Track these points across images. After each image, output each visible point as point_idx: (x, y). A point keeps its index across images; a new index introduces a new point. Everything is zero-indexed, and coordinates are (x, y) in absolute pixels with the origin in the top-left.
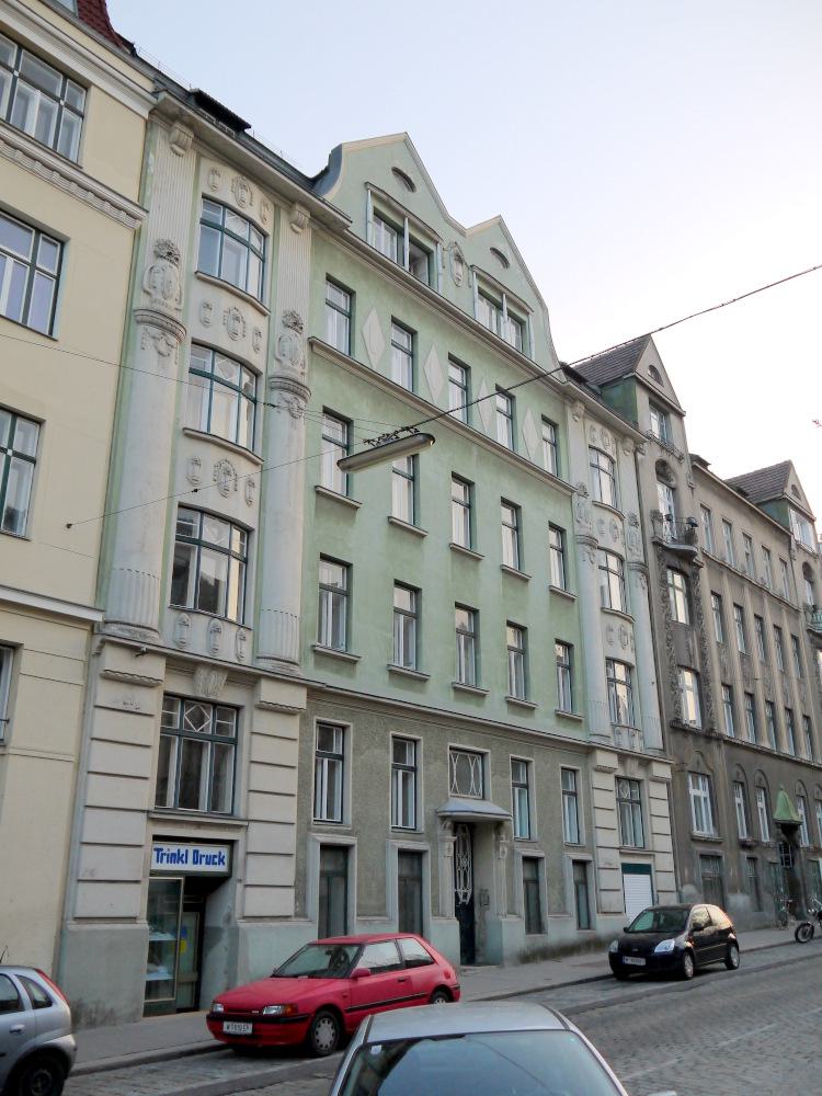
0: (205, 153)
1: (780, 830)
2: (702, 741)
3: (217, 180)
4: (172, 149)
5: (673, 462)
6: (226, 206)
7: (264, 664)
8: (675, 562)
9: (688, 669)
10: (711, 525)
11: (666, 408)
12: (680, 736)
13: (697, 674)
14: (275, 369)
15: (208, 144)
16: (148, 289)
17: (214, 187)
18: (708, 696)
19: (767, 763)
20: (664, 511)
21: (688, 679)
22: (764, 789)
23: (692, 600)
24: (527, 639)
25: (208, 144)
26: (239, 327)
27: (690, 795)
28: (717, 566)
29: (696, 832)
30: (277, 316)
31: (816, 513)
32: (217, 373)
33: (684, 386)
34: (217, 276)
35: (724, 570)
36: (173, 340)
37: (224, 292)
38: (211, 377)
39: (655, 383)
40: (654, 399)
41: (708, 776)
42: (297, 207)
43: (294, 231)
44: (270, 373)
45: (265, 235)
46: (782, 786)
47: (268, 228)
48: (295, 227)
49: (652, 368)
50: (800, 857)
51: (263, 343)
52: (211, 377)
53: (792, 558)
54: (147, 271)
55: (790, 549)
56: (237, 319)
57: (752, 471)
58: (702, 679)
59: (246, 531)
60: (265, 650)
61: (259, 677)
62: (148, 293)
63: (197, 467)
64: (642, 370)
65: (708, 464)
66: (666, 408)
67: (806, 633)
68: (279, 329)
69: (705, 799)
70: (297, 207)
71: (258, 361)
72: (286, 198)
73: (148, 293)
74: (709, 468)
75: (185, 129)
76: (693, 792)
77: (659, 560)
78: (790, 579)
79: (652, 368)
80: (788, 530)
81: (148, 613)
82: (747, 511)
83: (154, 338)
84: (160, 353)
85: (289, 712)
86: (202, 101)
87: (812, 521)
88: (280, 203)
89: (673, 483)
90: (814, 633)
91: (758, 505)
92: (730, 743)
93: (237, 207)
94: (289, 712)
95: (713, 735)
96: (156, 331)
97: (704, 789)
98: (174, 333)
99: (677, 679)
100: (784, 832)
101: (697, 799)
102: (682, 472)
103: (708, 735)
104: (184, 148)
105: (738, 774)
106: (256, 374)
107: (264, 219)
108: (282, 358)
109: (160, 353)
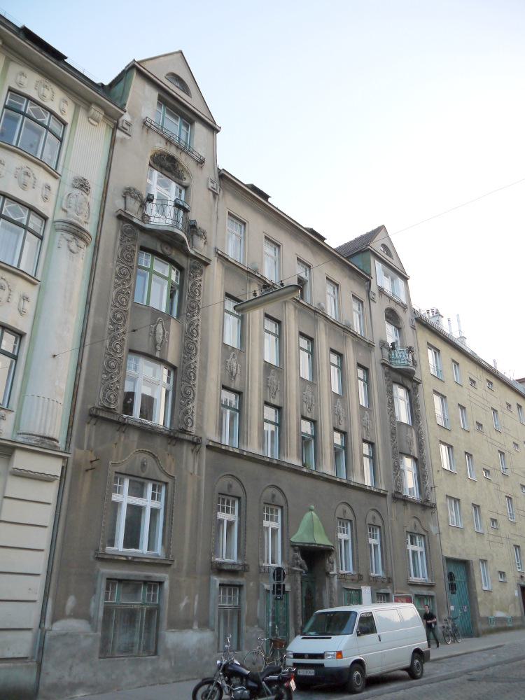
0: (14, 58)
1: (298, 555)
2: (419, 509)
3: (23, 80)
4: (89, 121)
5: (399, 311)
6: (29, 98)
7: (20, 439)
8: (399, 378)
9: (409, 456)
10: (279, 259)
11: (190, 115)
12: (400, 505)
13: (416, 460)
14: (61, 216)
15: (20, 54)
16: (65, 208)
17: (20, 84)
18: (424, 476)
19: (285, 480)
20: (390, 341)
21: (408, 463)
22: (282, 507)
23: (413, 405)
24: (22, 344)
25: (20, 54)
26: (30, 181)
27: (408, 550)
28: (245, 274)
29: (413, 579)
30: (68, 177)
31: (409, 272)
32: (30, 226)
33: (407, 257)
34: (14, 144)
35: (349, 335)
36: (82, 243)
37: (42, 169)
38: (26, 228)
39: (387, 257)
40: (162, 94)
41: (424, 536)
42: (93, 106)
43: (90, 123)
44: (56, 219)
45: (65, 124)
46: (313, 507)
47: (67, 118)
48: (92, 121)
49: (384, 246)
50: (331, 584)
51: (52, 198)
52: (26, 228)
53: (370, 299)
54: (66, 196)
55: (368, 291)
56: (27, 174)
57: (352, 238)
58: (419, 462)
59: (20, 335)
60: (24, 429)
61: (14, 448)
62: (65, 211)
63: (26, 302)
64: (376, 246)
65: (325, 239)
66: (190, 115)
67: (380, 368)
68: (67, 189)
69: (421, 553)
70: (93, 106)
71: (48, 213)
72: (87, 101)
73: (65, 211)
74: (270, 200)
75: (98, 109)
76: (410, 547)
77: (386, 376)
78: (367, 317)
79: (384, 246)
80: (369, 275)
81: (50, 429)
82: (308, 242)
83: (68, 240)
84: (71, 251)
85: (45, 479)
86: (27, 34)
87: (405, 279)
88: (78, 102)
89: (185, 182)
90: (390, 368)
91: (347, 258)
92: (215, 448)
93: (40, 100)
94: (45, 479)
95: (428, 504)
96: (70, 236)
97: (421, 545)
98: (82, 239)
99: (398, 463)
100: (304, 556)
101: (414, 553)
102: (406, 318)
103: (178, 436)
104: (98, 122)
105: (374, 518)
106: (45, 219)
107: (63, 111)
108: (68, 210)
109: (71, 251)
